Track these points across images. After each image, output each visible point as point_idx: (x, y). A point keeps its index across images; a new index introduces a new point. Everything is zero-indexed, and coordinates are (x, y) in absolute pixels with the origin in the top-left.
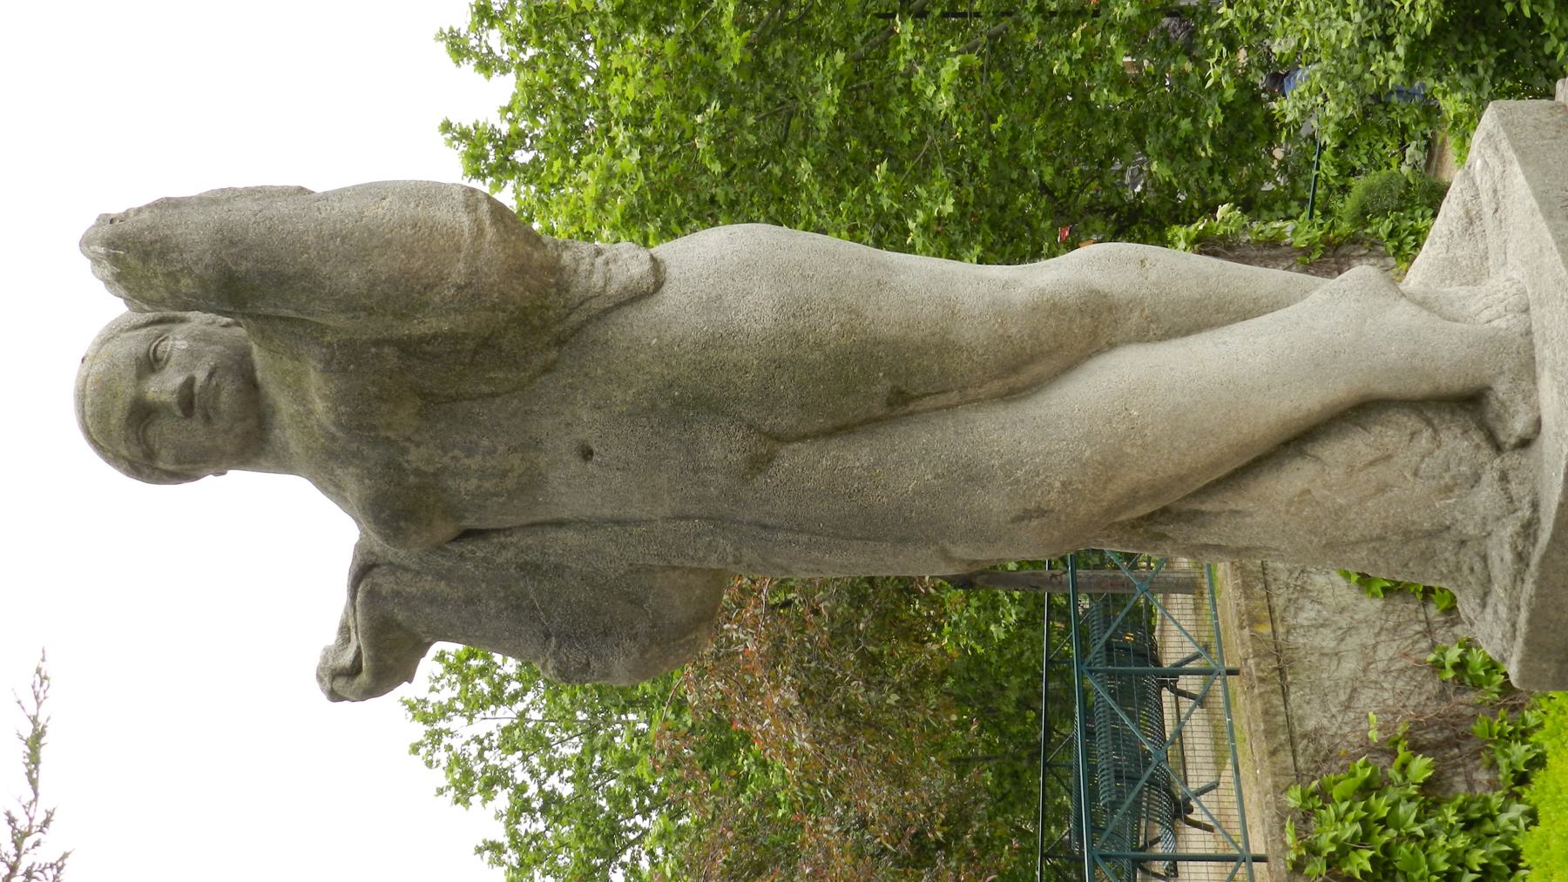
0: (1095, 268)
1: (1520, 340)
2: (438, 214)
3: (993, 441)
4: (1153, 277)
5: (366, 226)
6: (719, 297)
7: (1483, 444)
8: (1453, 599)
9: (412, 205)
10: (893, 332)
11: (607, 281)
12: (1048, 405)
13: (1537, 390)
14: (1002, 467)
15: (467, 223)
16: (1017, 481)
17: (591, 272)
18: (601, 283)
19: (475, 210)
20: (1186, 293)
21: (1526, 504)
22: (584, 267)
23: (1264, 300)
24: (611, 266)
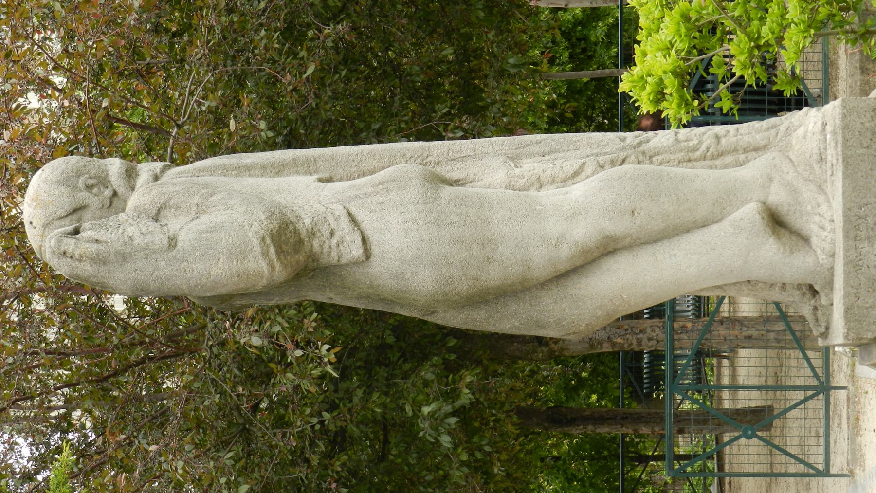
0: (607, 219)
1: (827, 272)
2: (249, 264)
3: (550, 310)
4: (638, 222)
5: (213, 281)
6: (402, 273)
7: (807, 292)
8: (823, 98)
9: (235, 262)
10: (497, 283)
11: (340, 257)
12: (579, 288)
13: (832, 293)
14: (554, 322)
15: (265, 267)
16: (563, 325)
17: (330, 252)
18: (336, 258)
19: (267, 255)
20: (656, 228)
21: (824, 324)
22: (326, 249)
23: (700, 221)
24: (341, 247)
